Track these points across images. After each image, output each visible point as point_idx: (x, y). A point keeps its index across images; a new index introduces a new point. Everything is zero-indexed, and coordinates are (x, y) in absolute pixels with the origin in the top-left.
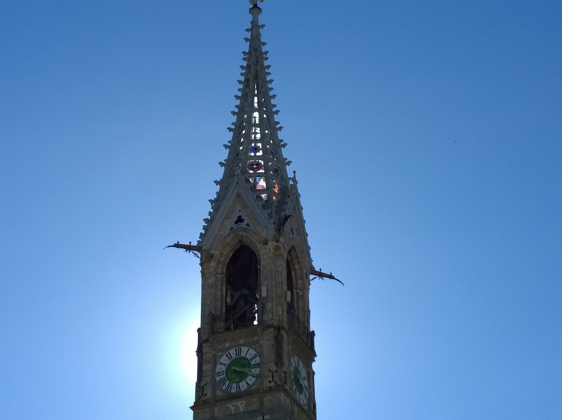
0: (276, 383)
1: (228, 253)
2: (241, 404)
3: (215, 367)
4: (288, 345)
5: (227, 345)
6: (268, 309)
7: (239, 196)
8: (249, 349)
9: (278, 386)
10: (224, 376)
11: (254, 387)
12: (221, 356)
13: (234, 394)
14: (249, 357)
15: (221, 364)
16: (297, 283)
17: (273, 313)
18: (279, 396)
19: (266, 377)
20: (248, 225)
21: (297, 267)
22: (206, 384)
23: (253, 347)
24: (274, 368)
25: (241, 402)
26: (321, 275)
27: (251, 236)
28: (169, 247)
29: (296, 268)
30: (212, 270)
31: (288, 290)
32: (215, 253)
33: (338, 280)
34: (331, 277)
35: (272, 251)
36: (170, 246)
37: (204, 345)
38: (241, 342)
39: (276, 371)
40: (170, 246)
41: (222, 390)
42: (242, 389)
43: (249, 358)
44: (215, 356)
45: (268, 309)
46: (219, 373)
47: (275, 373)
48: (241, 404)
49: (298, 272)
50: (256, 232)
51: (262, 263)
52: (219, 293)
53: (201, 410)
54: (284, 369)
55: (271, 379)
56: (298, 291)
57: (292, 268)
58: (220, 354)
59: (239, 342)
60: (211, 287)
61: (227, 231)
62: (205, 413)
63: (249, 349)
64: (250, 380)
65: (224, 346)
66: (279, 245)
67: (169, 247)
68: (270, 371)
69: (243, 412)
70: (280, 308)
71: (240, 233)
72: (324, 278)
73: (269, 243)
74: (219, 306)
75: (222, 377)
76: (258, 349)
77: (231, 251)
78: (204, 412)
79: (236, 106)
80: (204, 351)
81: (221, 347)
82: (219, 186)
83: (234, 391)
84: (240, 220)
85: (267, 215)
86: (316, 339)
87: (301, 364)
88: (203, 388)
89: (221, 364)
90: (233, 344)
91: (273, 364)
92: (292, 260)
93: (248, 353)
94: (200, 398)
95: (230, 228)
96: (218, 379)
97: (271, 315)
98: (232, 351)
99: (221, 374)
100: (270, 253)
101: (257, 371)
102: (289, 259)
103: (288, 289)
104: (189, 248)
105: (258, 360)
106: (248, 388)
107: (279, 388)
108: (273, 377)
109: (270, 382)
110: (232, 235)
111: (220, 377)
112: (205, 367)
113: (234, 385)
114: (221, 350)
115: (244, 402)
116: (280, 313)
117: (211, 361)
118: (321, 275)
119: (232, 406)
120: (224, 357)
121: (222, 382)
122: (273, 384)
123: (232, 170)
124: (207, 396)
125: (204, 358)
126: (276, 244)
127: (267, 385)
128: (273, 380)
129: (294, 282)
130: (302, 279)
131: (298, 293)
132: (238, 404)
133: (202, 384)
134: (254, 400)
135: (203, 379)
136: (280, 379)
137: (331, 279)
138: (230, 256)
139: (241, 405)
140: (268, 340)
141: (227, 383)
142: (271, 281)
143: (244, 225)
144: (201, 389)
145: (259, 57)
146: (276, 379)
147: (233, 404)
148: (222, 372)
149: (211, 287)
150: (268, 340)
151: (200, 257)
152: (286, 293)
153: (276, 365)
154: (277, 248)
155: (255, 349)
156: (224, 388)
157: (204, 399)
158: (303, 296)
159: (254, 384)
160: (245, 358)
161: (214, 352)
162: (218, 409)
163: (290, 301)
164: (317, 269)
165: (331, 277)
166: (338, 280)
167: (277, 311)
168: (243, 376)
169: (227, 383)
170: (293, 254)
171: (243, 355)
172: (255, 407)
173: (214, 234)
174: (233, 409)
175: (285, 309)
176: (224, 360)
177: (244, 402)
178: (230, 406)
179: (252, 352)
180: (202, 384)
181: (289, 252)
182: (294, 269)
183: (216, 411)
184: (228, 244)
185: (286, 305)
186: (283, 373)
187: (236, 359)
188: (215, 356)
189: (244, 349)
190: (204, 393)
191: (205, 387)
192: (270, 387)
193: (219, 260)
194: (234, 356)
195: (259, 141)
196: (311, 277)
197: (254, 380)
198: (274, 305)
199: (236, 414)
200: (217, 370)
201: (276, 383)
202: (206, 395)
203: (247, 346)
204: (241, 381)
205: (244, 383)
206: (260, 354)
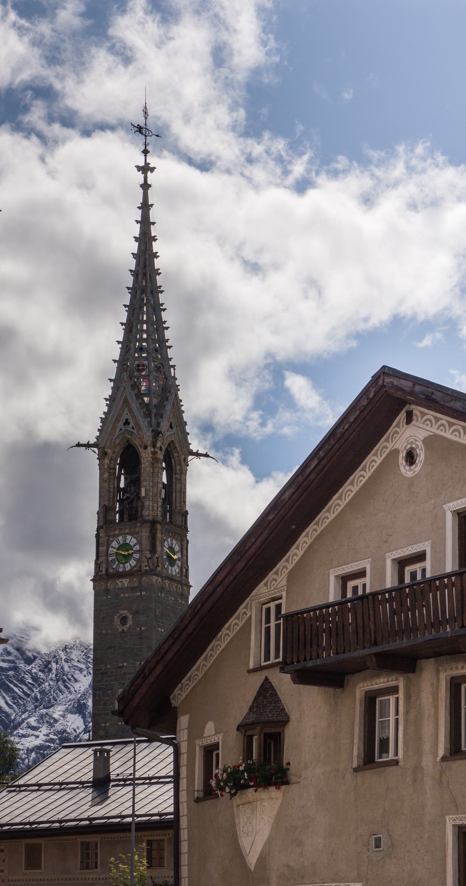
1: (119, 450)
2: (126, 581)
5: (117, 532)
6: (146, 507)
7: (126, 401)
8: (132, 538)
9: (152, 570)
10: (114, 557)
11: (136, 569)
13: (121, 572)
14: (132, 544)
15: (112, 547)
16: (176, 469)
17: (149, 510)
18: (152, 578)
19: (144, 562)
20: (133, 428)
21: (176, 455)
22: (101, 563)
23: (135, 536)
24: (149, 556)
25: (125, 580)
26: (197, 455)
27: (135, 440)
28: (72, 447)
29: (175, 456)
30: (106, 466)
31: (163, 489)
32: (109, 451)
33: (212, 458)
35: (150, 455)
36: (73, 447)
37: (101, 530)
38: (127, 531)
39: (150, 558)
40: (73, 447)
41: (113, 568)
42: (127, 569)
44: (108, 540)
45: (146, 507)
46: (111, 554)
47: (149, 560)
48: (126, 581)
49: (177, 459)
52: (112, 486)
54: (157, 556)
55: (146, 564)
56: (177, 476)
57: (172, 457)
58: (111, 539)
59: (125, 531)
62: (101, 586)
63: (132, 538)
64: (133, 563)
65: (115, 533)
67: (72, 447)
69: (127, 587)
71: (127, 435)
72: (201, 457)
74: (111, 497)
75: (113, 557)
76: (138, 538)
77: (121, 449)
78: (100, 584)
80: (101, 535)
83: (121, 570)
85: (146, 423)
87: (174, 542)
88: (100, 565)
89: (112, 547)
90: (121, 532)
92: (171, 451)
93: (131, 540)
96: (110, 559)
97: (148, 511)
98: (120, 538)
99: (112, 555)
100: (148, 457)
101: (137, 556)
102: (169, 449)
104: (88, 446)
106: (131, 569)
108: (148, 562)
109: (146, 566)
110: (121, 437)
112: (101, 549)
113: (121, 566)
114: (113, 536)
116: (156, 508)
117: (105, 543)
119: (120, 582)
121: (113, 561)
122: (148, 568)
124: (103, 572)
125: (100, 541)
127: (144, 568)
128: (148, 565)
129: (174, 467)
130: (180, 464)
131: (176, 478)
132: (124, 581)
133: (99, 562)
134: (135, 579)
135: (100, 558)
137: (207, 458)
138: (120, 453)
139: (126, 582)
141: (117, 563)
143: (129, 428)
144: (98, 566)
146: (150, 565)
147: (120, 580)
148: (113, 554)
149: (106, 481)
150: (145, 532)
151: (97, 453)
152: (161, 490)
154: (154, 453)
155: (136, 538)
156: (114, 567)
157: (100, 574)
158: (180, 479)
160: (128, 544)
161: (107, 538)
163: (164, 497)
164: (195, 451)
166: (212, 458)
167: (153, 507)
168: (127, 558)
169: (117, 563)
170: (172, 446)
171: (128, 542)
172: (136, 584)
173: (107, 433)
174: (120, 584)
176: (115, 544)
177: (128, 580)
178: (118, 582)
180: (99, 562)
182: (174, 458)
183: (109, 584)
185: (161, 501)
187: (123, 544)
189: (129, 537)
190: (101, 569)
191: (101, 564)
192: (146, 570)
193: (111, 457)
194: (121, 542)
195: (145, 340)
197: (135, 563)
198: (151, 502)
199: (122, 588)
200: (109, 552)
202: (102, 571)
203: (131, 535)
204: (126, 563)
205: (127, 565)
206: (139, 542)
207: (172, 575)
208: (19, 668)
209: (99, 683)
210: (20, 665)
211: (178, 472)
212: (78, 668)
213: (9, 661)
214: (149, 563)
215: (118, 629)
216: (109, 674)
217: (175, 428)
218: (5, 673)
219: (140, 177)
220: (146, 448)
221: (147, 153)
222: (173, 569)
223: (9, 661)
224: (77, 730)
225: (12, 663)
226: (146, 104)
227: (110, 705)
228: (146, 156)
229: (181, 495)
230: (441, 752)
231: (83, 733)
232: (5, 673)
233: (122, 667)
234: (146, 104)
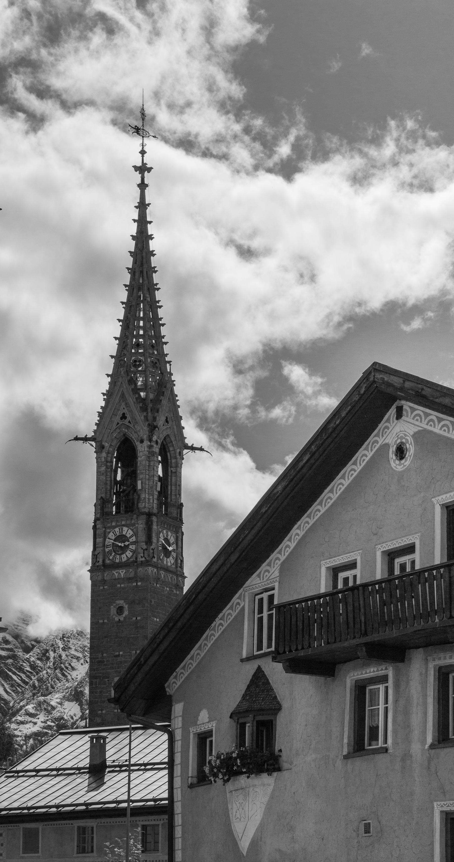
0: (146, 558)
1: (116, 443)
3: (105, 540)
4: (157, 526)
5: (114, 524)
6: (143, 499)
9: (147, 561)
10: (111, 548)
11: (132, 560)
12: (109, 532)
14: (128, 536)
15: (109, 539)
16: (171, 462)
17: (145, 502)
19: (139, 553)
21: (171, 449)
22: (98, 554)
23: (131, 527)
24: (145, 547)
26: (193, 448)
28: (70, 441)
32: (106, 445)
33: (207, 452)
34: (201, 449)
37: (98, 522)
38: (123, 523)
39: (146, 549)
41: (109, 559)
42: (123, 560)
43: (128, 537)
44: (105, 532)
46: (108, 546)
47: (145, 551)
48: (122, 572)
49: (172, 452)
50: (135, 431)
51: (139, 459)
53: (95, 573)
54: (152, 547)
55: (142, 555)
56: (172, 469)
60: (103, 474)
61: (114, 426)
62: (98, 576)
64: (129, 554)
65: (111, 524)
66: (152, 444)
67: (70, 441)
68: (142, 549)
69: (124, 578)
70: (151, 497)
73: (145, 442)
78: (97, 575)
79: (98, 420)
80: (98, 526)
81: (109, 525)
82: (109, 378)
83: (117, 561)
84: (124, 417)
85: (143, 418)
86: (184, 509)
87: (169, 533)
88: (97, 556)
89: (109, 539)
90: (118, 524)
91: (144, 543)
93: (128, 532)
94: (95, 563)
95: (116, 423)
96: (107, 550)
97: (144, 504)
98: (117, 530)
99: (109, 546)
100: (145, 451)
101: (133, 547)
103: (159, 480)
105: (134, 539)
107: (147, 563)
108: (144, 553)
109: (142, 557)
110: (118, 431)
111: (108, 548)
112: (98, 540)
113: (118, 556)
114: (110, 528)
115: (124, 571)
117: (102, 535)
118: (193, 448)
119: (116, 572)
120: (111, 534)
121: (110, 553)
122: (143, 559)
123: (123, 353)
126: (149, 443)
127: (140, 559)
128: (144, 556)
129: (169, 461)
130: (176, 458)
135: (97, 549)
136: (149, 555)
137: (201, 452)
139: (122, 573)
140: (141, 524)
142: (144, 475)
143: (126, 422)
144: (95, 557)
145: (144, 241)
147: (117, 571)
148: (109, 545)
149: (103, 474)
152: (157, 483)
153: (146, 544)
154: (150, 447)
155: (132, 530)
156: (111, 558)
157: (97, 564)
159: (131, 558)
160: (125, 536)
161: (104, 529)
162: (106, 574)
164: (190, 445)
165: (201, 449)
166: (207, 452)
167: (149, 499)
169: (113, 554)
171: (124, 533)
172: (132, 575)
174: (116, 575)
175: (156, 497)
176: (111, 535)
177: (124, 571)
178: (115, 573)
179: (130, 532)
181: (165, 438)
182: (169, 451)
183: (105, 575)
184: (116, 438)
186: (151, 550)
187: (119, 536)
188: (105, 532)
189: (125, 529)
191: (98, 555)
193: (108, 450)
194: (118, 534)
196: (185, 451)
197: (131, 554)
198: (147, 495)
199: (118, 579)
201: (146, 558)
202: (99, 562)
203: (127, 527)
204: (123, 554)
205: (124, 556)
206: (136, 534)
207: (168, 567)
208: (18, 657)
209: (96, 672)
210: (19, 654)
211: (173, 465)
212: (75, 656)
213: (8, 650)
214: (145, 554)
215: (114, 618)
216: (105, 663)
217: (170, 422)
218: (4, 661)
219: (137, 177)
220: (142, 441)
221: (144, 154)
222: (168, 560)
223: (8, 650)
224: (74, 717)
225: (11, 652)
226: (143, 105)
227: (107, 693)
228: (143, 156)
229: (176, 487)
230: (429, 740)
231: (80, 720)
232: (4, 661)
233: (119, 655)
234: (143, 105)
